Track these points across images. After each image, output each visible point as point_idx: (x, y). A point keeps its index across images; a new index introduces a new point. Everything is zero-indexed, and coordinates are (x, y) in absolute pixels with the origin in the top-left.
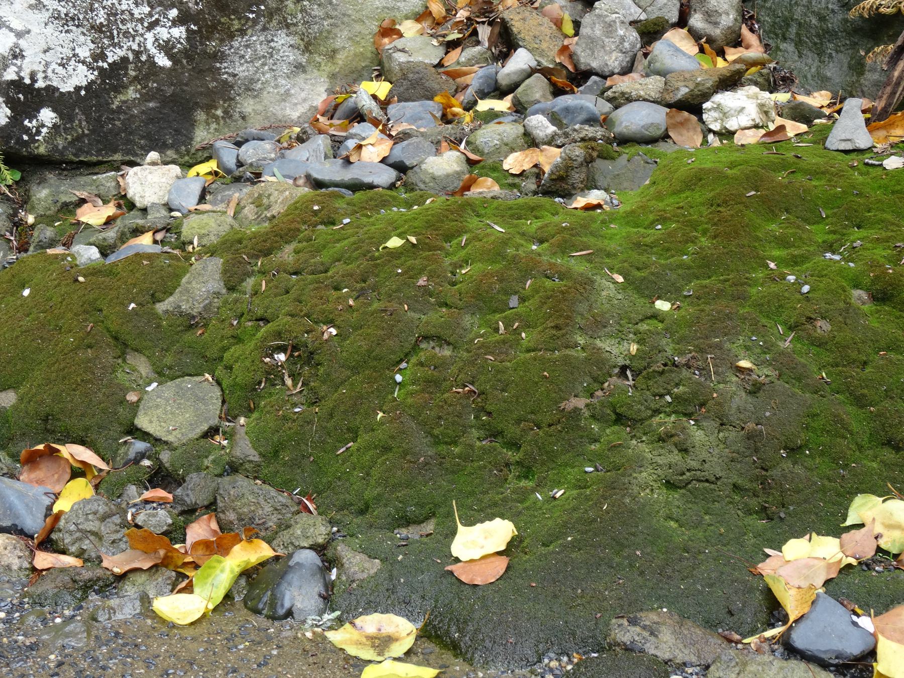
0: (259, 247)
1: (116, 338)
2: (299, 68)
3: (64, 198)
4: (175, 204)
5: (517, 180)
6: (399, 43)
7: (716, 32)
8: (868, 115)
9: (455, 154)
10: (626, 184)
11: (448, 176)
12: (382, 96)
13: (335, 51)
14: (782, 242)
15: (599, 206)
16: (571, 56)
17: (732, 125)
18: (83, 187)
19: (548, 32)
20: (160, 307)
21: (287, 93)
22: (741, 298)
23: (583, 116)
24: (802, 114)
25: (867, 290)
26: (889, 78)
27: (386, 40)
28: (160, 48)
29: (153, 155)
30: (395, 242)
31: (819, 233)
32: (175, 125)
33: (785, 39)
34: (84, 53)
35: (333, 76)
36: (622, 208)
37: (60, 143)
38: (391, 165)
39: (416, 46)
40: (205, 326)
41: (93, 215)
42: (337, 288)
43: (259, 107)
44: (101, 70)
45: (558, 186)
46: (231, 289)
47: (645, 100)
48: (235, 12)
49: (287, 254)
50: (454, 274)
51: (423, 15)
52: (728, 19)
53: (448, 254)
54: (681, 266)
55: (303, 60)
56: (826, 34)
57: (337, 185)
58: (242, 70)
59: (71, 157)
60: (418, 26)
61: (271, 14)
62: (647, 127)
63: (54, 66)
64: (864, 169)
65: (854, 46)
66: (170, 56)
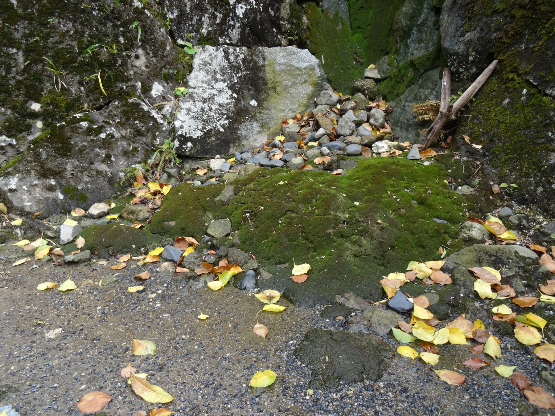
2: (260, 132)
4: (223, 170)
6: (288, 126)
7: (377, 124)
12: (282, 141)
13: (270, 128)
14: (393, 186)
15: (340, 174)
16: (336, 130)
17: (380, 151)
18: (198, 164)
20: (216, 199)
21: (256, 139)
23: (337, 148)
29: (218, 156)
30: (281, 183)
31: (404, 183)
33: (397, 126)
34: (200, 127)
35: (269, 135)
37: (193, 152)
39: (292, 126)
41: (201, 172)
42: (265, 195)
44: (204, 132)
45: (329, 167)
46: (236, 195)
48: (242, 116)
49: (252, 185)
51: (295, 118)
53: (296, 187)
54: (363, 192)
56: (409, 125)
58: (244, 133)
61: (252, 117)
66: (224, 128)
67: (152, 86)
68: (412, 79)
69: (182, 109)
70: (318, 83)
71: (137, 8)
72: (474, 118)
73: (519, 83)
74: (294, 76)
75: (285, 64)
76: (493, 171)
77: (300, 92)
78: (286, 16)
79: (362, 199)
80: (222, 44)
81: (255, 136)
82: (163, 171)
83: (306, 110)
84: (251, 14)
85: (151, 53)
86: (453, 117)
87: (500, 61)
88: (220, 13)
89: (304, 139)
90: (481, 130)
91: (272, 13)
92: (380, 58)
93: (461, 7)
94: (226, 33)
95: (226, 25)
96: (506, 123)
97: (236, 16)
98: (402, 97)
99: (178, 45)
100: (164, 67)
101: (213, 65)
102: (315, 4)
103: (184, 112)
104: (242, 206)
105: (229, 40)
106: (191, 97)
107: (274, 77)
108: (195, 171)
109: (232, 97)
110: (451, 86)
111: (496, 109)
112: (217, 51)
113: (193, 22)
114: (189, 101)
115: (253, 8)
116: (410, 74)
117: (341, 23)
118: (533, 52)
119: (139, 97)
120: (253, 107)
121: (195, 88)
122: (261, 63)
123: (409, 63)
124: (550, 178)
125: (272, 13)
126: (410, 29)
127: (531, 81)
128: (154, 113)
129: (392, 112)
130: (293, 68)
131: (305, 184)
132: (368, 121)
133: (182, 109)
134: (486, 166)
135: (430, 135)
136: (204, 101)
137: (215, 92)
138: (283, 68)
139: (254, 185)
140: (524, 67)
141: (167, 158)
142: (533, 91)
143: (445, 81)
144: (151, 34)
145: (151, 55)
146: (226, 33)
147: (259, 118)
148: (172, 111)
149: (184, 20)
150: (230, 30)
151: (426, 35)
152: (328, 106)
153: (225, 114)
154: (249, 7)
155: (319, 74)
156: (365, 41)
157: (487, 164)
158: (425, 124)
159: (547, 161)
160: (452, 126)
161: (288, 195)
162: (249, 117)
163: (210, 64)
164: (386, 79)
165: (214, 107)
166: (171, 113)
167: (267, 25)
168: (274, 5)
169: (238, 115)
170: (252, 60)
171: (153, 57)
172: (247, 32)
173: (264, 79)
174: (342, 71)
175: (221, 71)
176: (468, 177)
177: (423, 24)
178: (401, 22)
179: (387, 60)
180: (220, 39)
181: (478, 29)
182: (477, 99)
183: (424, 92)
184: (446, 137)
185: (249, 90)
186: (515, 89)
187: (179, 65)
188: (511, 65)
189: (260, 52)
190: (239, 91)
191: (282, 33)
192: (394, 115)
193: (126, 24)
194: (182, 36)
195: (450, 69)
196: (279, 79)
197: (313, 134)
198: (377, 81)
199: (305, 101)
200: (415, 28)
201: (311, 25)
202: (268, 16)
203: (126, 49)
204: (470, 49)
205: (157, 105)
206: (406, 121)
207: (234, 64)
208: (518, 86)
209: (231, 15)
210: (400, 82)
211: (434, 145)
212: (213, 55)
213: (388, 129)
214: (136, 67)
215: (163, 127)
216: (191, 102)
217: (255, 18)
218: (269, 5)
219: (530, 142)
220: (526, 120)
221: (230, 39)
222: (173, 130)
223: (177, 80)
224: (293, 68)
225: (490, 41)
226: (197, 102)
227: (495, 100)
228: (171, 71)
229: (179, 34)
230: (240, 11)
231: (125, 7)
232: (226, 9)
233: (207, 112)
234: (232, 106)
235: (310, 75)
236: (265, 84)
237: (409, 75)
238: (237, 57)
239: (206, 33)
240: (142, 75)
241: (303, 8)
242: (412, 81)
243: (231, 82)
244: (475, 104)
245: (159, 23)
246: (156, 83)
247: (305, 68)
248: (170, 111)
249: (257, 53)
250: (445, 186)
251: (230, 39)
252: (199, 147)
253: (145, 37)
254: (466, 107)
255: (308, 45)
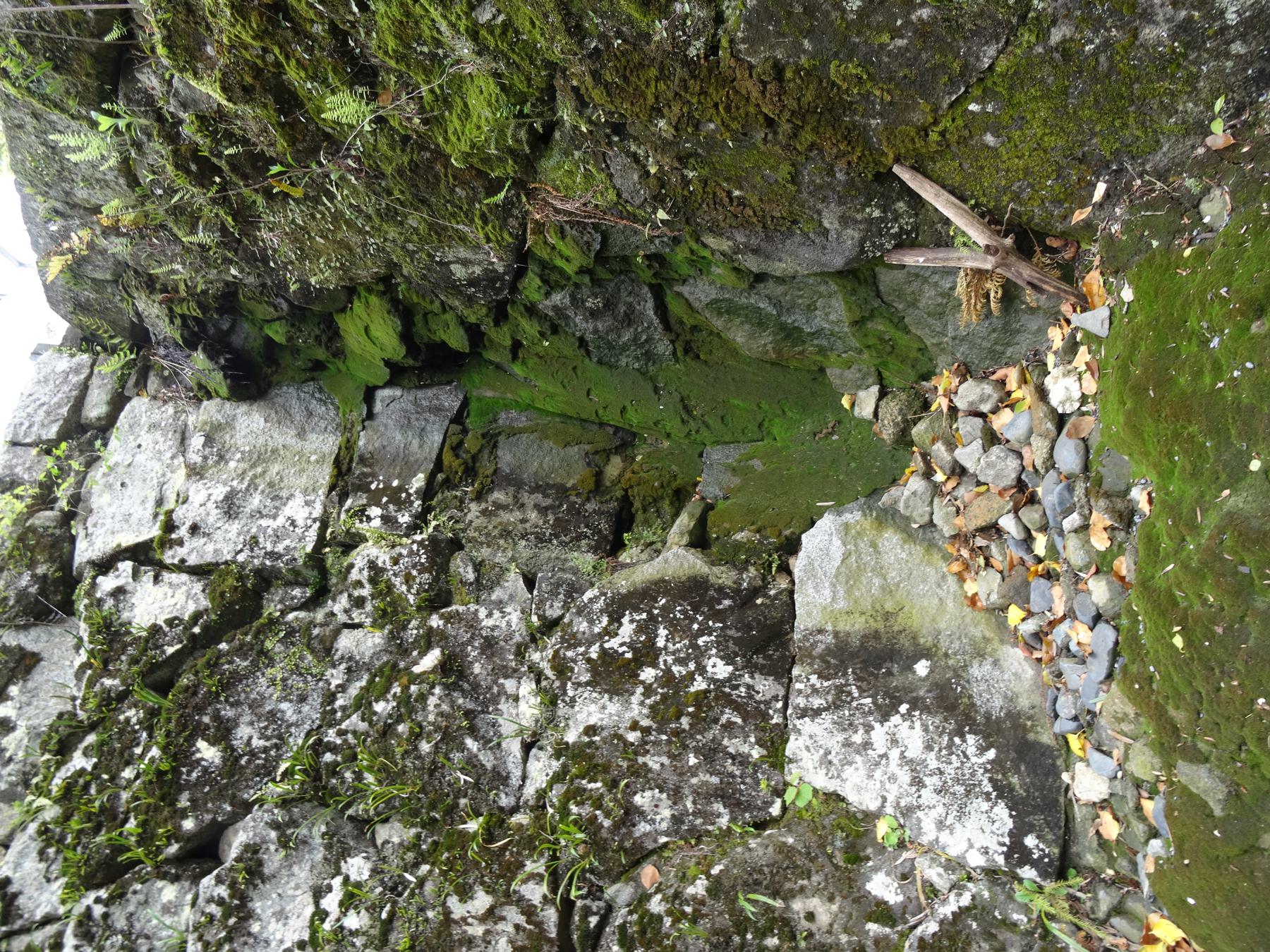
0: (1170, 733)
1: (1245, 852)
2: (996, 663)
3: (1095, 844)
4: (1112, 774)
5: (1116, 543)
6: (982, 596)
7: (996, 396)
8: (1078, 309)
9: (1091, 582)
10: (1125, 471)
11: (1110, 590)
12: (1022, 614)
13: (984, 638)
14: (1197, 375)
15: (1149, 494)
16: (1005, 489)
17: (1077, 395)
18: (1086, 830)
19: (985, 502)
20: (1218, 812)
21: (1015, 674)
22: (1252, 409)
23: (1066, 494)
24: (1071, 348)
25: (1252, 321)
26: (1054, 294)
27: (979, 604)
28: (981, 754)
29: (1065, 777)
30: (1178, 641)
31: (1188, 349)
32: (1038, 755)
33: (1003, 353)
34: (985, 806)
35: (1002, 642)
36: (1155, 479)
37: (1050, 837)
38: (1095, 625)
39: (986, 586)
40: (1238, 785)
41: (1111, 829)
42: (1219, 689)
43: (1025, 696)
44: (998, 797)
45: (1126, 517)
46: (1207, 760)
47: (1052, 449)
48: (956, 699)
49: (1179, 716)
50: (1211, 606)
51: (961, 578)
52: (988, 389)
53: (1191, 606)
54: (1217, 448)
55: (990, 660)
56: (1006, 328)
57: (1112, 667)
58: (998, 702)
59: (1062, 832)
60: (968, 581)
61: (958, 676)
62: (1078, 453)
63: (994, 828)
64: (1130, 314)
65: (1016, 311)
66: (988, 748)
67: (875, 897)
68: (891, 321)
69: (937, 840)
70: (877, 518)
71: (708, 890)
72: (1016, 198)
73: (953, 120)
74: (861, 568)
75: (834, 586)
76: (1165, 149)
77: (898, 561)
78: (733, 574)
79: (1240, 452)
80: (785, 718)
81: (1006, 677)
82: (1103, 923)
83: (940, 549)
84: (727, 647)
85: (800, 882)
86: (1008, 241)
87: (897, 160)
88: (722, 713)
89: (1022, 562)
90: (1049, 182)
91: (727, 602)
92: (830, 384)
93: (768, 238)
94: (762, 706)
95: (747, 704)
96: (1044, 134)
97: (729, 680)
98: (929, 342)
99: (782, 816)
100: (830, 857)
101: (829, 746)
102: (711, 513)
103: (944, 837)
104: (1248, 751)
105: (777, 701)
106: (908, 811)
107: (862, 613)
108: (1106, 841)
109: (908, 716)
110: (927, 247)
111: (1005, 158)
112: (799, 732)
113: (738, 773)
114: (919, 820)
115: (717, 642)
116: (879, 326)
117: (750, 462)
118: (891, 103)
119: (904, 936)
120: (932, 671)
121: (884, 799)
122: (830, 639)
123: (854, 329)
124: (1211, 32)
125: (727, 602)
126: (782, 327)
127: (954, 98)
128: (947, 910)
129: (965, 364)
130: (843, 569)
131: (1184, 585)
132: (982, 415)
133: (937, 840)
134: (1148, 167)
135: (1045, 287)
136: (918, 783)
137: (895, 754)
138: (841, 593)
139: (1177, 708)
140: (921, 114)
141: (1066, 905)
142: (977, 92)
143: (915, 259)
144: (761, 872)
145: (805, 882)
146: (762, 706)
147: (959, 661)
148: (940, 865)
149: (734, 793)
150: (758, 697)
151: (801, 297)
152: (936, 500)
153: (951, 739)
154: (714, 651)
155: (858, 515)
156: (789, 414)
157: (1143, 164)
158: (1010, 294)
159: (1160, 43)
160: (1025, 239)
161: (1220, 630)
162: (958, 685)
163: (828, 753)
164: (880, 374)
165: (933, 764)
166: (946, 868)
167: (750, 615)
168: (712, 598)
169: (951, 706)
170: (822, 657)
171: (809, 878)
172: (761, 661)
173: (865, 636)
174: (853, 465)
175: (845, 730)
176: (1176, 202)
177: (777, 304)
178: (765, 345)
179: (838, 371)
180: (774, 721)
181: (820, 206)
182: (972, 196)
183: (929, 298)
184: (1048, 250)
185: (889, 673)
186: (966, 126)
187: (826, 822)
188: (913, 141)
189: (806, 638)
190: (892, 697)
191: (765, 586)
192: (974, 358)
193: (742, 924)
194: (764, 802)
195: (888, 251)
196: (866, 604)
197: (1010, 542)
198: (883, 394)
199: (918, 550)
200: (783, 319)
201: (753, 524)
202: (732, 613)
203: (793, 938)
204: (859, 217)
205: (922, 898)
206: (995, 335)
207: (830, 698)
208: (960, 122)
209: (727, 690)
210: (892, 347)
211: (1069, 274)
212: (809, 742)
213: (1012, 375)
214: (831, 925)
215: (982, 896)
216: (920, 814)
217: (737, 641)
218: (711, 608)
219: (1103, 83)
220: (1047, 96)
221: (776, 698)
222: (991, 873)
223: (859, 835)
224: (843, 569)
225: (850, 184)
226: (921, 801)
227: (982, 162)
228: (839, 844)
229: (760, 809)
230: (720, 669)
231: (707, 915)
232: (717, 698)
233: (945, 782)
234: (933, 721)
235: (858, 533)
236: (876, 635)
237: (881, 328)
238: (815, 691)
239: (761, 750)
240: (850, 915)
241: (717, 538)
242: (896, 320)
243: (870, 713)
244: (983, 200)
245: (739, 850)
246: (869, 886)
247: (844, 544)
248: (941, 870)
249: (807, 644)
250: (1201, 255)
251: (776, 698)
252: (1038, 819)
253: (767, 888)
254: (990, 217)
255: (793, 533)
